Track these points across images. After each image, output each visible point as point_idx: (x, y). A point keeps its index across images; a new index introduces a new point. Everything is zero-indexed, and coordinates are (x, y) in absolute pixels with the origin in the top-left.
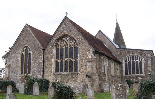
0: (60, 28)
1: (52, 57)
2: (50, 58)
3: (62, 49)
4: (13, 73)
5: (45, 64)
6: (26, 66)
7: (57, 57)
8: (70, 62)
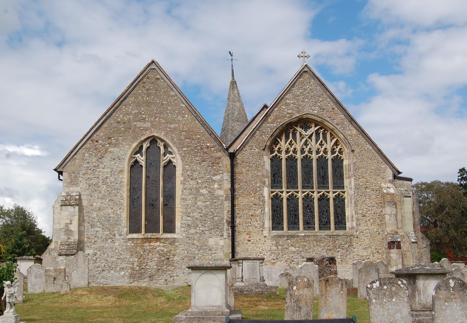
0: (287, 96)
1: (264, 183)
2: (256, 183)
3: (291, 160)
4: (97, 229)
5: (236, 202)
6: (152, 205)
7: (275, 181)
8: (319, 200)
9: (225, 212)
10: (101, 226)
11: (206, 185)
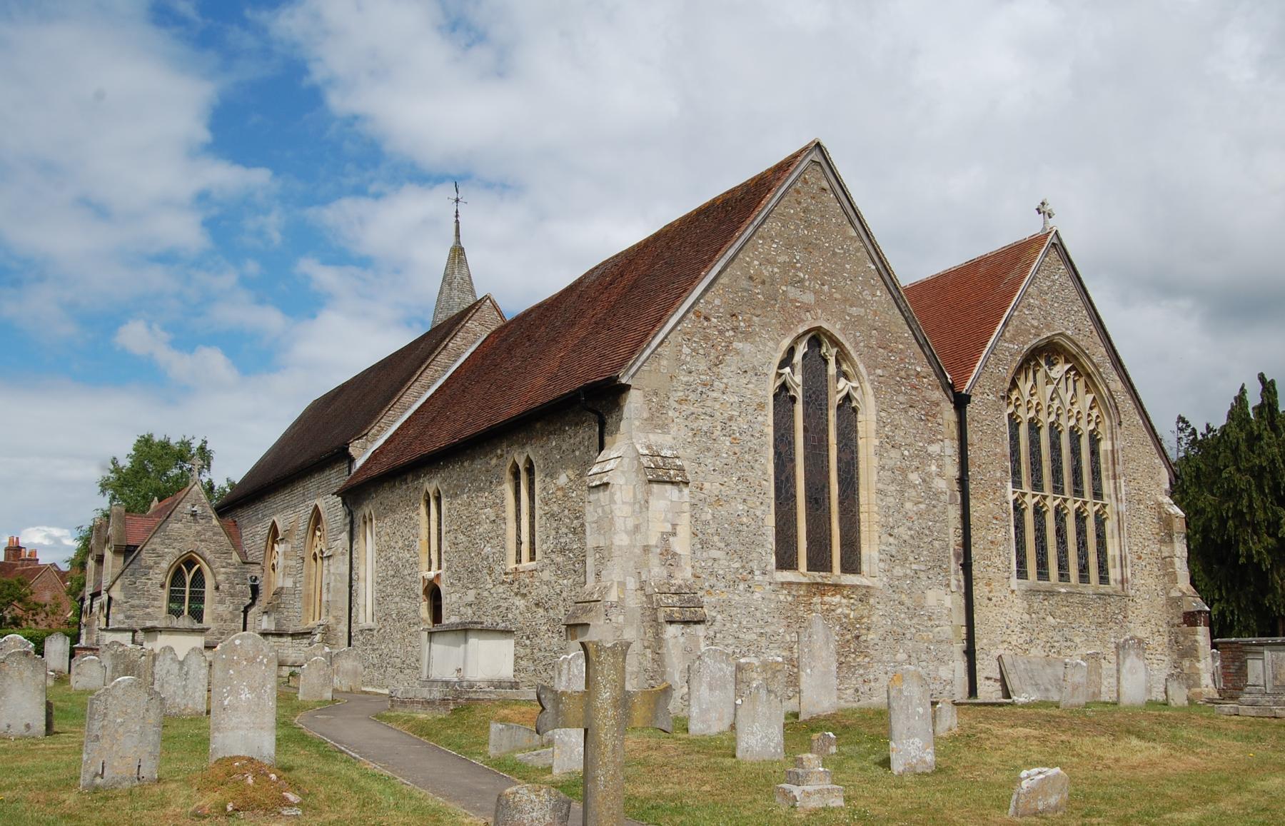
4: (714, 553)
9: (951, 530)
10: (722, 545)
11: (916, 463)
